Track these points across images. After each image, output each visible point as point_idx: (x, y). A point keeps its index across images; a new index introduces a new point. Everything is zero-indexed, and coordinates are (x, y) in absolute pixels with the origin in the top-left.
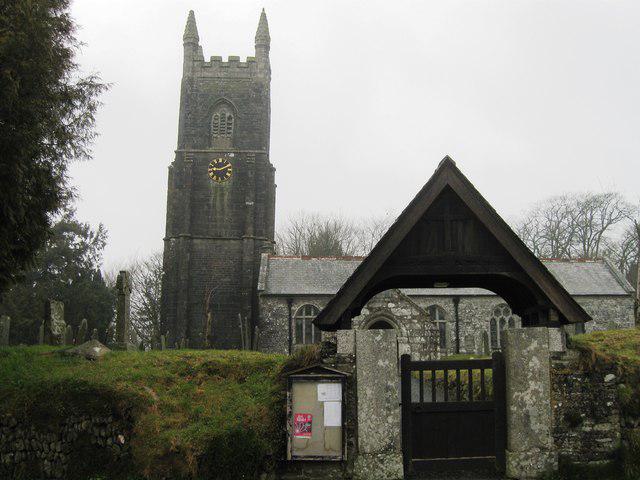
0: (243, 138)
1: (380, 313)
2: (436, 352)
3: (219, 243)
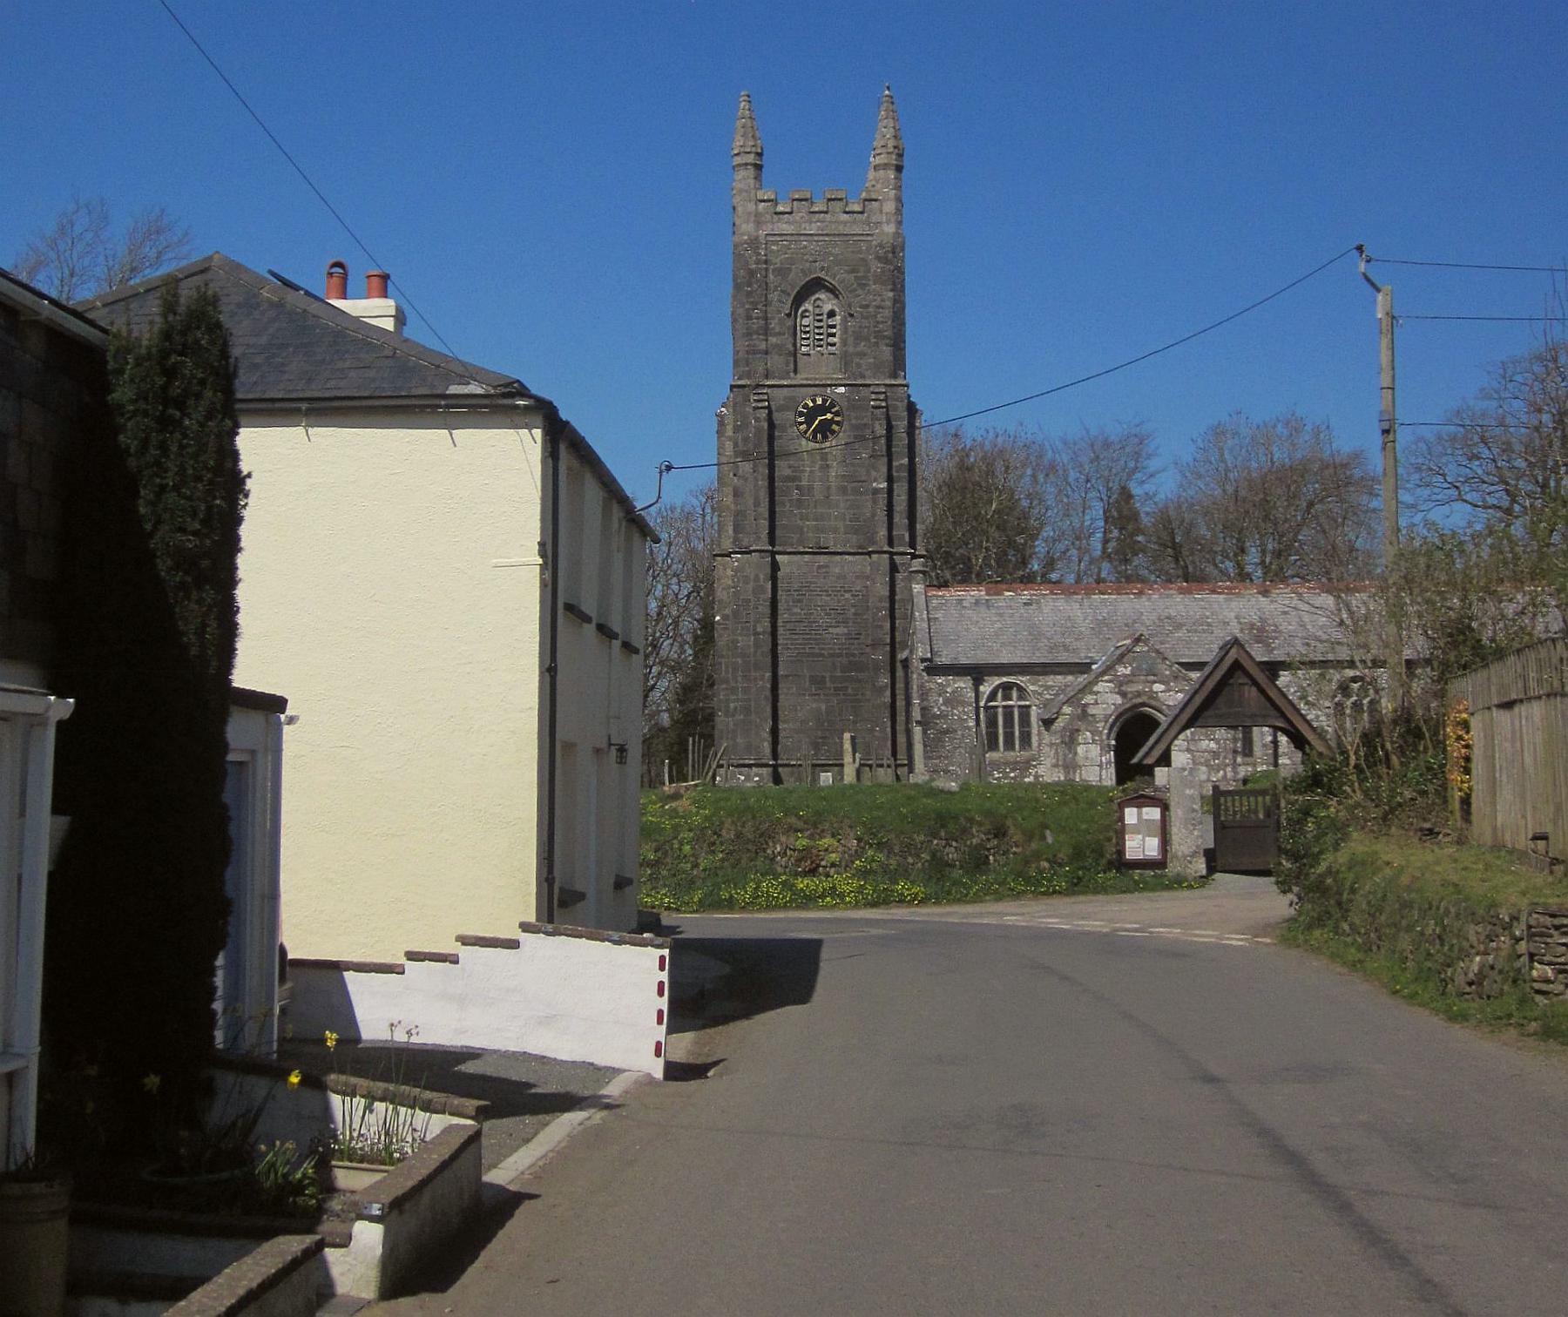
0: (862, 355)
2: (1235, 765)
3: (823, 559)
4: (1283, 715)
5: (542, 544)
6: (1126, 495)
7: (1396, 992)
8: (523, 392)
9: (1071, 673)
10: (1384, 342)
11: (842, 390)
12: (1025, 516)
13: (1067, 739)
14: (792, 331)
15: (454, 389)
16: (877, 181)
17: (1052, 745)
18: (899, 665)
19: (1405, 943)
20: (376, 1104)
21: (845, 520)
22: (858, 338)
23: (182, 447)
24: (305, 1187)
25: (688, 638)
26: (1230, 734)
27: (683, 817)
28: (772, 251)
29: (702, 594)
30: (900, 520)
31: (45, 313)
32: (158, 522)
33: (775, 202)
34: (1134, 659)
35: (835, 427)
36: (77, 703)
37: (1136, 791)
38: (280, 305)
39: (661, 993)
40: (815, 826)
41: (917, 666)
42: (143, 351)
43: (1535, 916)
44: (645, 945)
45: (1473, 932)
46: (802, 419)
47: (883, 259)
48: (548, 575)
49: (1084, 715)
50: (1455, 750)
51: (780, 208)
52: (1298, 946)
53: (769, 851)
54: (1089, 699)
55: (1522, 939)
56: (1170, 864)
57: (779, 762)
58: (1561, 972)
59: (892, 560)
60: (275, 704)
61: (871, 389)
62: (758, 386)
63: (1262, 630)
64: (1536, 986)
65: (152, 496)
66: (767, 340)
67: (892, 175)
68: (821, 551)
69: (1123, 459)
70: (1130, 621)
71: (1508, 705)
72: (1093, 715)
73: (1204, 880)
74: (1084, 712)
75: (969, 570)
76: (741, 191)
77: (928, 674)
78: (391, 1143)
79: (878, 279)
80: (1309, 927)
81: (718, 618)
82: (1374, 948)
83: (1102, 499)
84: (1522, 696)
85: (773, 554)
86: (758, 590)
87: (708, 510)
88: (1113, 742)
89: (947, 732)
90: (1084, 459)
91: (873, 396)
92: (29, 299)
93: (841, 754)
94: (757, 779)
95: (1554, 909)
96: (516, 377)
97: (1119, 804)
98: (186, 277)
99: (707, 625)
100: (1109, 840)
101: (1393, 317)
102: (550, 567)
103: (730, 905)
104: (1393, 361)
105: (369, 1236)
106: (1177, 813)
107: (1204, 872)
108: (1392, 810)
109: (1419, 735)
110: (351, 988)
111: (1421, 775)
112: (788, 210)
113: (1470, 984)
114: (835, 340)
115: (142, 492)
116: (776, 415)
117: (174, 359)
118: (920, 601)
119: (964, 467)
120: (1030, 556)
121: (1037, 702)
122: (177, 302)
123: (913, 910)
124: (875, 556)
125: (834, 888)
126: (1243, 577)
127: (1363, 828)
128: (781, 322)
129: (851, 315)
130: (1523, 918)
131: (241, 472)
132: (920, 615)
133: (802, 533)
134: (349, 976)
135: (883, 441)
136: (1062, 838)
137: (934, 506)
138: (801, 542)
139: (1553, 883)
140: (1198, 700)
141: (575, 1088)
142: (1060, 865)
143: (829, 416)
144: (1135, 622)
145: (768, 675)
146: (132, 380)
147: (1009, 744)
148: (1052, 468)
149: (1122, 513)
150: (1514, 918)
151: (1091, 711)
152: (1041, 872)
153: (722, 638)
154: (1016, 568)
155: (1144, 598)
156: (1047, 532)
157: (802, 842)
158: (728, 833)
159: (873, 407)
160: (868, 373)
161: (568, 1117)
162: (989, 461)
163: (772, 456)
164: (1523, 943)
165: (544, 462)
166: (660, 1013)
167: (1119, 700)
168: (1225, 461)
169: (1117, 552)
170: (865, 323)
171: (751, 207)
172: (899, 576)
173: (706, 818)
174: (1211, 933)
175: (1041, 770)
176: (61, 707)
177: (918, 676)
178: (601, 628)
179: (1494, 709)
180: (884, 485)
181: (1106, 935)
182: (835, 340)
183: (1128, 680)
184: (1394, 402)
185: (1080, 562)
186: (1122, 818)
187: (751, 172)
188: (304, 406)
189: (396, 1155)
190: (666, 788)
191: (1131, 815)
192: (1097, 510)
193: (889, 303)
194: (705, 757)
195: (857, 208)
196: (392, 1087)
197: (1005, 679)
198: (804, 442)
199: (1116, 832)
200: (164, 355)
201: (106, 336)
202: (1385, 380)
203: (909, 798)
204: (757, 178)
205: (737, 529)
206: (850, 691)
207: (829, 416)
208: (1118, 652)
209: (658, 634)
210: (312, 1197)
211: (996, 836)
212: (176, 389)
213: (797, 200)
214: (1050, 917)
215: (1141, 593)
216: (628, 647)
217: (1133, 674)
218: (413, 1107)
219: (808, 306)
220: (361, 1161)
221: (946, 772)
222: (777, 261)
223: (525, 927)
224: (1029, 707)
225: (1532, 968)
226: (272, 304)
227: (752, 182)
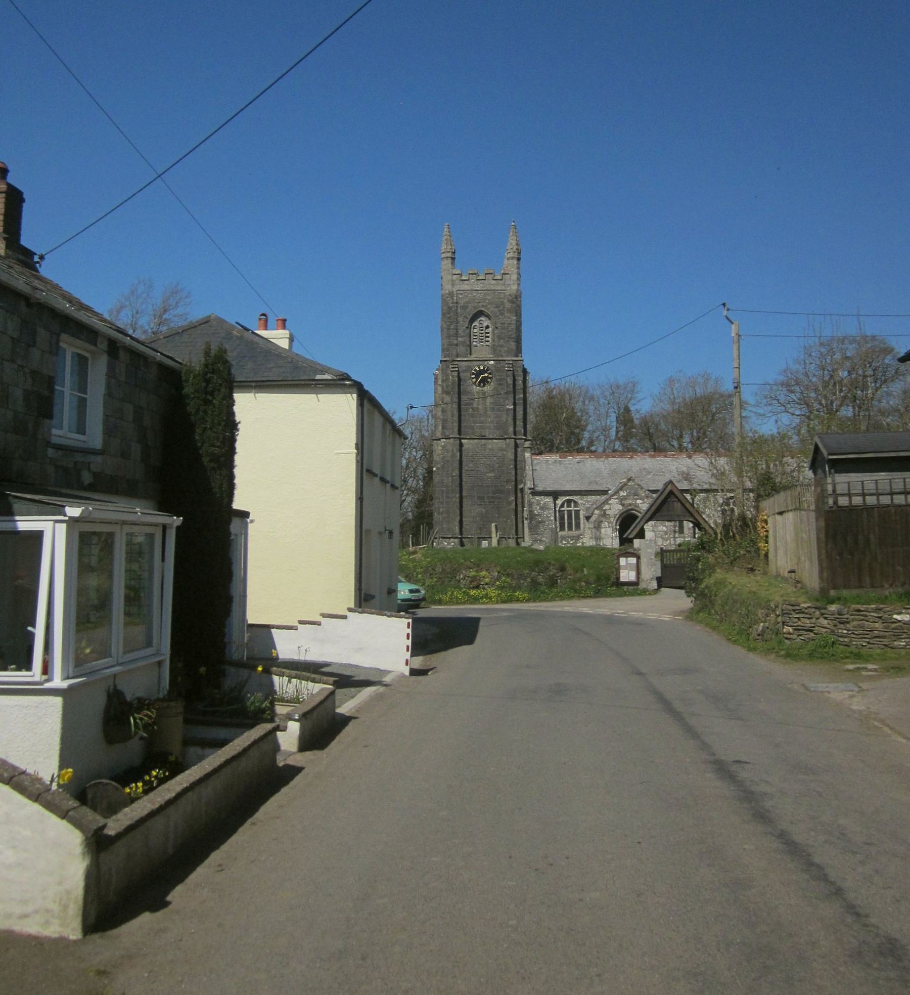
0: (501, 346)
1: (630, 508)
2: (675, 538)
3: (483, 441)
4: (693, 516)
5: (357, 444)
6: (627, 410)
7: (729, 639)
8: (348, 378)
9: (599, 495)
10: (735, 346)
11: (492, 362)
12: (579, 420)
13: (596, 525)
14: (468, 335)
15: (318, 377)
16: (508, 265)
17: (589, 528)
18: (519, 491)
19: (734, 618)
20: (293, 680)
21: (493, 423)
22: (500, 338)
23: (213, 411)
24: (267, 711)
25: (421, 477)
26: (672, 524)
27: (418, 562)
28: (459, 298)
29: (427, 456)
30: (520, 423)
31: (158, 359)
32: (203, 443)
33: (461, 275)
34: (628, 488)
35: (489, 380)
36: (184, 519)
37: (625, 550)
38: (241, 338)
39: (408, 638)
40: (479, 566)
41: (527, 491)
42: (197, 372)
43: (785, 606)
44: (401, 618)
45: (760, 613)
46: (473, 376)
47: (511, 302)
48: (359, 458)
49: (604, 515)
50: (762, 533)
51: (464, 278)
52: (693, 620)
53: (457, 578)
54: (606, 507)
55: (779, 616)
56: (640, 584)
57: (463, 536)
58: (795, 630)
59: (516, 443)
60: (245, 515)
61: (506, 362)
62: (454, 361)
63: (688, 474)
64: (785, 636)
65: (201, 432)
66: (457, 339)
67: (515, 262)
68: (483, 438)
69: (626, 393)
70: (626, 470)
71: (781, 513)
72: (609, 515)
73: (656, 591)
74: (605, 513)
75: (552, 446)
76: (445, 270)
77: (532, 495)
78: (299, 695)
79: (509, 311)
80: (699, 612)
81: (434, 469)
82: (724, 621)
83: (615, 412)
84: (786, 509)
85: (460, 439)
86: (453, 456)
87: (430, 417)
88: (618, 527)
89: (540, 522)
90: (607, 393)
91: (507, 366)
92: (152, 353)
93: (490, 533)
94: (453, 544)
95: (792, 603)
96: (346, 372)
97: (617, 556)
98: (200, 325)
99: (430, 471)
100: (613, 572)
101: (739, 336)
102: (360, 453)
103: (440, 602)
104: (739, 356)
105: (294, 727)
106: (644, 560)
107: (656, 587)
108: (735, 560)
109: (748, 526)
110: (275, 636)
111: (748, 544)
112: (467, 279)
113: (759, 635)
114: (489, 339)
115: (197, 430)
116: (462, 375)
117: (209, 375)
118: (528, 461)
119: (551, 397)
120: (582, 439)
121: (583, 508)
122: (210, 353)
123: (522, 604)
124: (507, 440)
125: (487, 594)
126: (681, 449)
127: (722, 567)
128: (464, 331)
129: (497, 328)
130: (780, 606)
131: (235, 421)
132: (528, 468)
133: (473, 429)
134: (273, 631)
135: (511, 386)
136: (591, 572)
137: (537, 416)
138: (473, 433)
139: (795, 592)
140: (653, 509)
141: (373, 679)
142: (591, 584)
143: (486, 375)
144: (628, 471)
145: (458, 495)
146: (192, 384)
147: (570, 528)
148: (592, 398)
149: (625, 418)
150: (777, 607)
151: (608, 512)
152: (581, 587)
153: (436, 478)
154: (575, 444)
155: (633, 460)
156: (589, 428)
157: (472, 573)
158: (439, 569)
159: (507, 371)
160: (504, 355)
161: (369, 688)
162: (562, 395)
163: (459, 393)
164: (780, 617)
165: (357, 409)
166: (408, 647)
167: (621, 507)
168: (673, 394)
169: (623, 436)
170: (503, 331)
171: (450, 277)
172: (519, 450)
173: (429, 563)
174: (655, 614)
175: (585, 540)
176: (177, 521)
177: (528, 497)
178: (383, 480)
179: (776, 515)
180: (512, 407)
181: (609, 616)
182: (489, 339)
183: (625, 498)
184: (739, 374)
185: (605, 441)
186: (618, 563)
187: (450, 261)
188: (253, 384)
189: (301, 700)
190: (410, 549)
191: (623, 561)
192: (613, 417)
193: (514, 322)
194: (429, 533)
195: (499, 277)
196: (299, 673)
197: (568, 498)
198: (475, 387)
199: (616, 569)
200: (205, 374)
201: (180, 366)
202: (736, 365)
203: (522, 553)
204: (453, 263)
205: (443, 428)
206: (496, 503)
207: (486, 375)
208: (621, 485)
209: (406, 476)
210: (269, 714)
211: (561, 571)
212: (210, 389)
213: (471, 274)
214: (584, 607)
215: (632, 457)
216: (393, 487)
217: (627, 495)
218: (307, 681)
219: (476, 323)
220: (286, 703)
221: (541, 541)
222: (462, 303)
223: (350, 610)
224: (579, 510)
225: (783, 628)
226: (238, 338)
227: (450, 265)
